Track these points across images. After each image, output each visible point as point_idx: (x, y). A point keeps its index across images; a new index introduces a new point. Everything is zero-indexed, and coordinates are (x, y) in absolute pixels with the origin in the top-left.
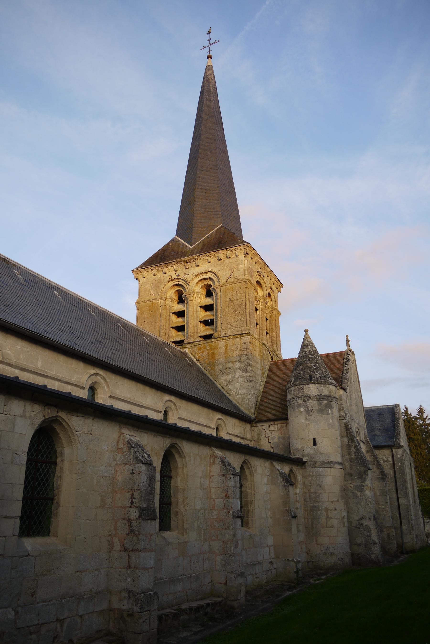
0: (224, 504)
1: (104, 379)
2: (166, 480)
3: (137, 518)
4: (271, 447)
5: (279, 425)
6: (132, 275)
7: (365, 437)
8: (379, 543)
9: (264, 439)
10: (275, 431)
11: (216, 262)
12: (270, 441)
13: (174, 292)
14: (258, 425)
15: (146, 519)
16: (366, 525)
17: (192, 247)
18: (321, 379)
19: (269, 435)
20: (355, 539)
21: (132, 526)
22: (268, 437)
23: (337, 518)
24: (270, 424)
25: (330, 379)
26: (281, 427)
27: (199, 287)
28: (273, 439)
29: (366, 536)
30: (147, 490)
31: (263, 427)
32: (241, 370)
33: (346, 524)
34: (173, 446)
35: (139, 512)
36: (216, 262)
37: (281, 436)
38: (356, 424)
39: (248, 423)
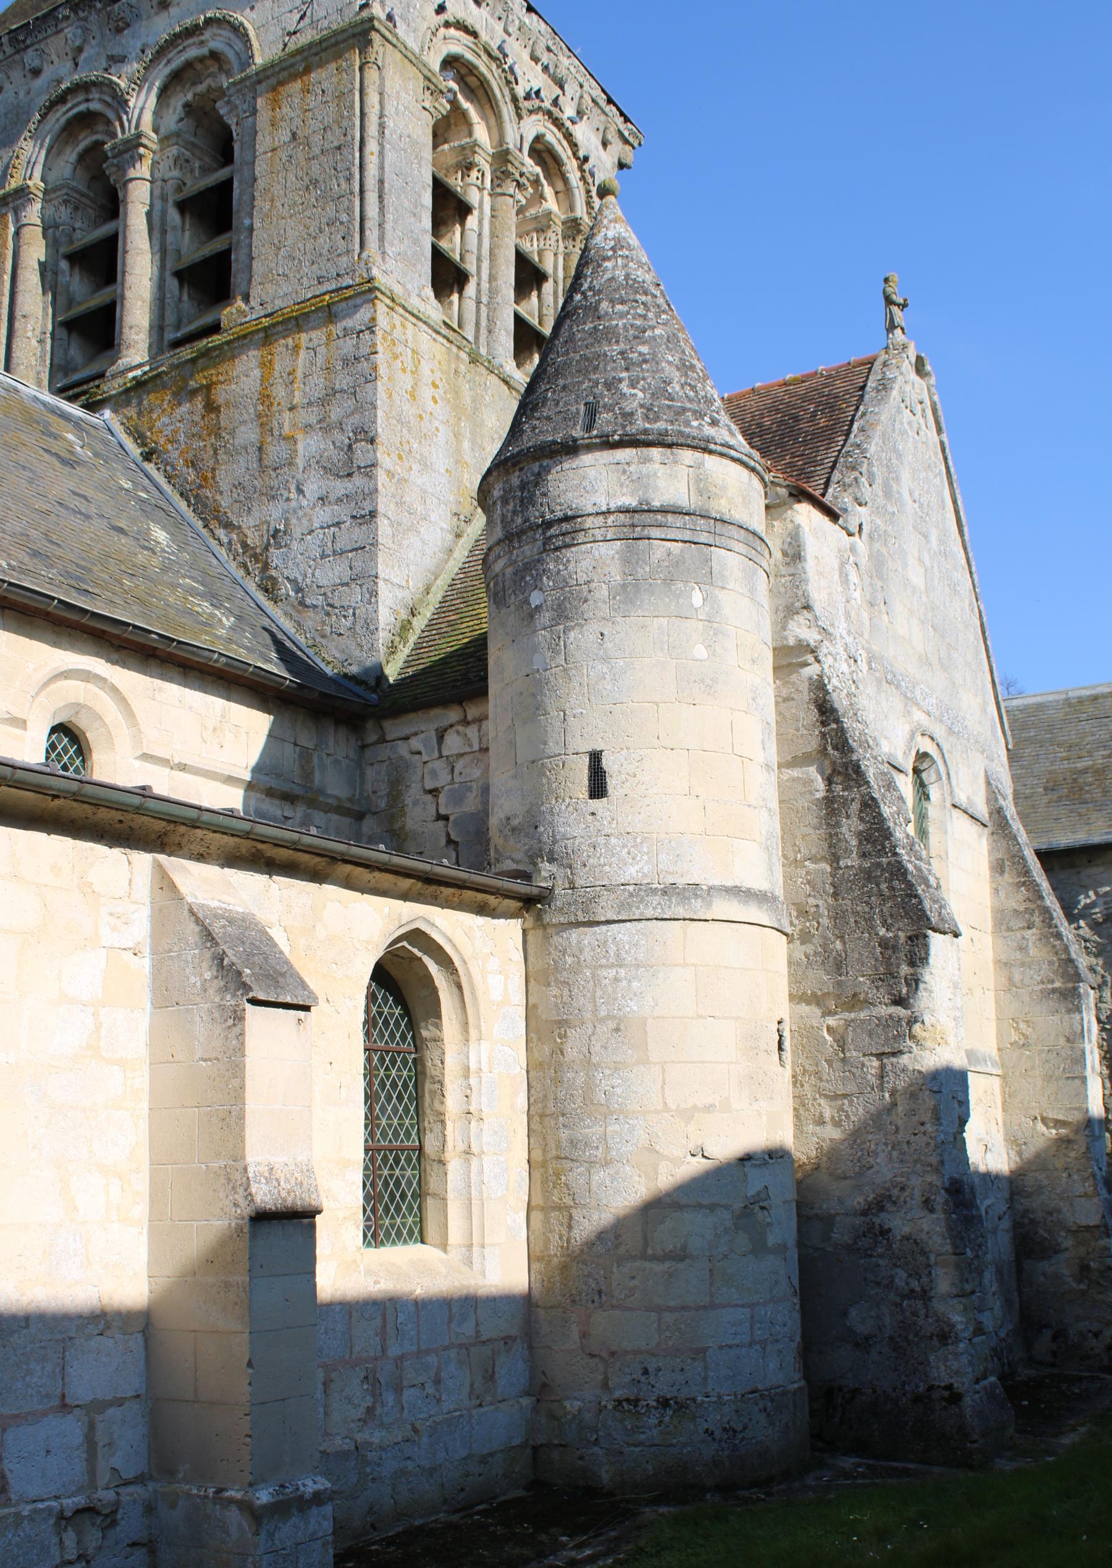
4: (450, 841)
9: (416, 803)
10: (468, 758)
14: (394, 728)
16: (906, 1238)
18: (647, 418)
19: (444, 779)
20: (845, 1314)
22: (434, 792)
23: (712, 1207)
24: (446, 723)
28: (457, 798)
29: (904, 1297)
31: (415, 743)
39: (338, 722)
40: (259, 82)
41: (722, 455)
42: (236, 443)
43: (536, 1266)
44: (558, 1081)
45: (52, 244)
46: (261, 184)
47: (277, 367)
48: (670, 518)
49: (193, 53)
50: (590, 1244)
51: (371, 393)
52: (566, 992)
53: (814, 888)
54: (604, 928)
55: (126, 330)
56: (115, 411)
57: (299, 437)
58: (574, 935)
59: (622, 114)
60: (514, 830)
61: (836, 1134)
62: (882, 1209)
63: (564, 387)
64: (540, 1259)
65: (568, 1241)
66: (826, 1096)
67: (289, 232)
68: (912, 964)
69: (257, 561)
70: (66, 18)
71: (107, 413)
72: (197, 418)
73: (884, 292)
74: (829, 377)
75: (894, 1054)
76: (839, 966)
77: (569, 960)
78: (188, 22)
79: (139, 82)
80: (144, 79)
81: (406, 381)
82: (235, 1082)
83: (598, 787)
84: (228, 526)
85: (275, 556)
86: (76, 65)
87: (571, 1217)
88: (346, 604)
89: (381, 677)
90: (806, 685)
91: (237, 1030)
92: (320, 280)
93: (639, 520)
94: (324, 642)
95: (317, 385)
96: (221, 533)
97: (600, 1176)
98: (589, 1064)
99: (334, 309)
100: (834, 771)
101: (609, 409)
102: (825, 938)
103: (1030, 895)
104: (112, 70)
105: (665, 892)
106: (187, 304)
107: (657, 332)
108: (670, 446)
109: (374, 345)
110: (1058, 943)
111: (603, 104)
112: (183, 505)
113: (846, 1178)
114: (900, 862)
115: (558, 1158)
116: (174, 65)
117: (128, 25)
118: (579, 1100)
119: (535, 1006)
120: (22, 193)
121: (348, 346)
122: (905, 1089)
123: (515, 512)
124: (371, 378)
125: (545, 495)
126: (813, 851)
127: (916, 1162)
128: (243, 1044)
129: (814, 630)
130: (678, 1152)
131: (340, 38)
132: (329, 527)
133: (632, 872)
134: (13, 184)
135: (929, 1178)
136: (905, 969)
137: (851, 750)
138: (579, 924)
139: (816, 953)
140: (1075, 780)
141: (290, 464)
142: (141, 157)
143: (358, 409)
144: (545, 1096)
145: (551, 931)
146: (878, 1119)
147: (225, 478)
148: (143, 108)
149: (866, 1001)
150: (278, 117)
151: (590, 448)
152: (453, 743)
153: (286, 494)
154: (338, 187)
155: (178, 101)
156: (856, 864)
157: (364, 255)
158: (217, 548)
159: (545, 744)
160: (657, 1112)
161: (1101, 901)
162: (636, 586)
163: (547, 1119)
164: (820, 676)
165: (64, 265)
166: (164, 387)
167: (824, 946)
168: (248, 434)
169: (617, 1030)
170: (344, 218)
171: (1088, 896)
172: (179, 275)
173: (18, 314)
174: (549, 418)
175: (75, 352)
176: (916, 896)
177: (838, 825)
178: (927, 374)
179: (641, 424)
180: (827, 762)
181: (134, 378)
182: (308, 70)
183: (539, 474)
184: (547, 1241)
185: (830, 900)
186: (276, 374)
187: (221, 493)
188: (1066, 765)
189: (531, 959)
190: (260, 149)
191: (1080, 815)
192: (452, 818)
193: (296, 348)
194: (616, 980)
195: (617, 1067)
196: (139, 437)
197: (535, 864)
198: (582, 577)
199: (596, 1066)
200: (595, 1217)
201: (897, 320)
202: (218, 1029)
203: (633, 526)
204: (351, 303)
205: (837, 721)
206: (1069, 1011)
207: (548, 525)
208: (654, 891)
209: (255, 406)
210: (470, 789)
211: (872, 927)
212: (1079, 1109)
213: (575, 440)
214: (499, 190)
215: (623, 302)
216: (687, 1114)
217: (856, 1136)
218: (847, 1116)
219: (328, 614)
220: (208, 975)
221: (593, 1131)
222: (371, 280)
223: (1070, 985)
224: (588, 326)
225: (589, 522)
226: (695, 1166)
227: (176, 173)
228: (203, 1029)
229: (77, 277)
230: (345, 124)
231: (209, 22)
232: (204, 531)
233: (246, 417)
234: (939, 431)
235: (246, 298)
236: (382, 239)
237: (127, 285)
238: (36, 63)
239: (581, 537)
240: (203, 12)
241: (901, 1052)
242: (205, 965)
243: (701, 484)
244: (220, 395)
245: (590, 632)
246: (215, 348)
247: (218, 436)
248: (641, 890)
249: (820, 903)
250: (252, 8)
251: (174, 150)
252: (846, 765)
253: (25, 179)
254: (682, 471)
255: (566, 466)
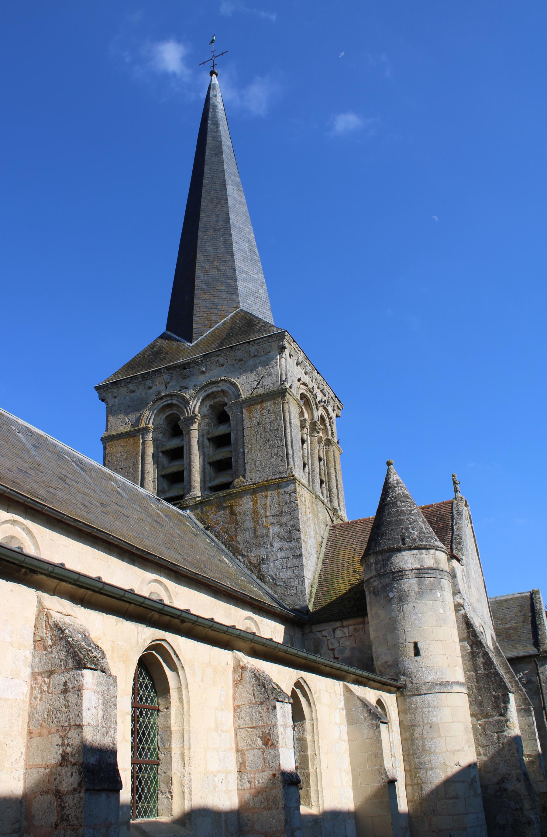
0: (264, 759)
1: (29, 532)
2: (147, 714)
3: (74, 789)
5: (351, 628)
6: (96, 395)
7: (494, 644)
8: (538, 822)
11: (233, 365)
12: (336, 656)
13: (164, 417)
14: (315, 628)
15: (94, 790)
16: (513, 791)
17: (193, 344)
19: (336, 645)
21: (63, 808)
22: (333, 650)
23: (463, 781)
24: (335, 627)
25: (436, 540)
26: (355, 630)
27: (206, 406)
28: (342, 651)
30: (98, 725)
31: (324, 633)
32: (282, 539)
33: (479, 791)
34: (157, 647)
35: (80, 774)
36: (233, 365)
37: (354, 646)
38: (479, 619)
40: (243, 403)
41: (440, 550)
42: (245, 527)
43: (410, 804)
44: (413, 744)
45: (156, 447)
46: (246, 438)
47: (259, 502)
48: (430, 571)
49: (215, 389)
50: (428, 795)
51: (296, 514)
52: (413, 716)
53: (470, 680)
54: (424, 696)
55: (193, 482)
56: (191, 511)
57: (270, 527)
58: (414, 698)
59: (338, 400)
60: (389, 666)
61: (485, 758)
62: (503, 782)
63: (392, 530)
64: (411, 801)
65: (421, 795)
66: (481, 746)
67: (259, 456)
68: (504, 703)
69: (256, 568)
70: (164, 372)
71: (188, 512)
72: (227, 517)
73: (453, 480)
74: (437, 507)
75: (502, 732)
76: (480, 704)
77: (413, 706)
78: (214, 380)
79: (194, 397)
80: (196, 396)
81: (304, 507)
82: (379, 745)
83: (417, 653)
84: (243, 555)
85: (263, 567)
86: (167, 387)
87: (422, 787)
88: (293, 585)
89: (308, 610)
90: (461, 617)
91: (378, 730)
92: (273, 474)
93: (422, 571)
94: (285, 597)
95: (276, 509)
96: (240, 558)
97: (430, 773)
98: (423, 738)
99: (280, 484)
100: (473, 643)
101: (408, 537)
102: (475, 696)
103: (510, 676)
104: (182, 391)
105: (440, 684)
106: (212, 474)
107: (415, 511)
108: (427, 549)
109: (296, 498)
110: (521, 692)
111: (334, 398)
112: (224, 547)
113: (490, 772)
114: (497, 672)
115: (415, 768)
116: (207, 393)
117: (189, 377)
118: (421, 750)
119: (402, 721)
120: (146, 429)
121: (287, 497)
122: (507, 743)
123: (380, 568)
124: (296, 509)
125: (392, 563)
126: (469, 668)
127: (513, 766)
128: (380, 734)
129: (462, 599)
130: (452, 764)
131: (274, 393)
132: (284, 558)
133: (430, 678)
134: (142, 425)
135: (518, 771)
136: (502, 705)
137: (478, 637)
138: (416, 695)
139: (473, 701)
140: (507, 632)
141: (267, 536)
142: (195, 422)
143: (292, 519)
144: (409, 749)
145: (406, 697)
146: (499, 753)
147: (241, 538)
148: (196, 405)
149: (491, 715)
150: (252, 416)
151: (405, 550)
152: (338, 633)
153: (266, 546)
154: (277, 443)
155: (208, 403)
156: (483, 672)
157: (289, 467)
158: (239, 563)
159: (399, 639)
160: (445, 752)
161: (525, 676)
162: (423, 592)
163: (410, 757)
164: (466, 614)
165: (161, 454)
166: (212, 504)
167: (475, 698)
168: (249, 524)
169: (431, 727)
170: (281, 453)
171: (520, 675)
172: (210, 464)
173: (146, 472)
174: (389, 539)
175: (165, 486)
176: (504, 682)
177: (476, 660)
178: (468, 506)
179: (419, 543)
180: (470, 641)
181: (199, 500)
182: (262, 402)
183: (389, 557)
184: (414, 795)
185: (476, 684)
186: (259, 504)
187: (239, 544)
188: (502, 626)
189: (400, 706)
190: (245, 426)
191: (512, 645)
192: (340, 659)
193: (266, 496)
194: (429, 712)
195: (432, 739)
196: (203, 521)
197: (398, 677)
198: (406, 589)
199: (425, 739)
200: (430, 786)
201: (458, 489)
202: (371, 730)
203: (420, 574)
204: (286, 483)
205: (473, 628)
206: (528, 716)
207: (394, 573)
208: (437, 684)
209: (251, 515)
210: (346, 649)
211: (491, 692)
212: (535, 750)
213: (401, 548)
214: (312, 435)
215: (404, 502)
216: (454, 752)
217: (492, 758)
218: (489, 752)
219: (286, 588)
220: (366, 715)
221: (426, 759)
222: (293, 476)
223: (527, 707)
224: (395, 510)
225: (407, 573)
226: (457, 769)
227: (207, 428)
228: (366, 730)
229: (165, 459)
230: (278, 422)
231: (221, 380)
232: (233, 557)
233: (248, 518)
234: (471, 523)
235: (244, 477)
236: (294, 461)
237: (192, 466)
238: (151, 385)
239: (405, 577)
240: (219, 377)
241: (504, 731)
242: (365, 713)
243: (436, 561)
244: (237, 509)
245: (411, 605)
246: (233, 493)
247: (237, 524)
248: (434, 684)
249: (473, 685)
250: (238, 378)
251: (207, 420)
252: (477, 642)
253: (146, 424)
254: (431, 556)
255: (398, 555)
